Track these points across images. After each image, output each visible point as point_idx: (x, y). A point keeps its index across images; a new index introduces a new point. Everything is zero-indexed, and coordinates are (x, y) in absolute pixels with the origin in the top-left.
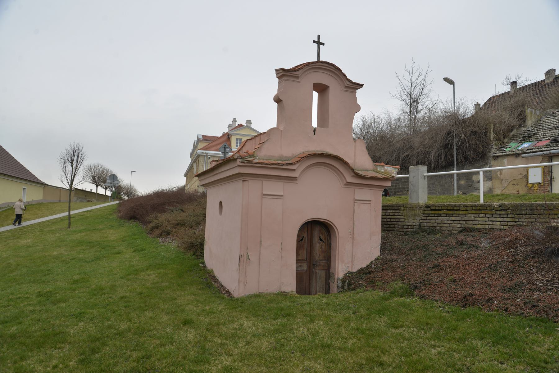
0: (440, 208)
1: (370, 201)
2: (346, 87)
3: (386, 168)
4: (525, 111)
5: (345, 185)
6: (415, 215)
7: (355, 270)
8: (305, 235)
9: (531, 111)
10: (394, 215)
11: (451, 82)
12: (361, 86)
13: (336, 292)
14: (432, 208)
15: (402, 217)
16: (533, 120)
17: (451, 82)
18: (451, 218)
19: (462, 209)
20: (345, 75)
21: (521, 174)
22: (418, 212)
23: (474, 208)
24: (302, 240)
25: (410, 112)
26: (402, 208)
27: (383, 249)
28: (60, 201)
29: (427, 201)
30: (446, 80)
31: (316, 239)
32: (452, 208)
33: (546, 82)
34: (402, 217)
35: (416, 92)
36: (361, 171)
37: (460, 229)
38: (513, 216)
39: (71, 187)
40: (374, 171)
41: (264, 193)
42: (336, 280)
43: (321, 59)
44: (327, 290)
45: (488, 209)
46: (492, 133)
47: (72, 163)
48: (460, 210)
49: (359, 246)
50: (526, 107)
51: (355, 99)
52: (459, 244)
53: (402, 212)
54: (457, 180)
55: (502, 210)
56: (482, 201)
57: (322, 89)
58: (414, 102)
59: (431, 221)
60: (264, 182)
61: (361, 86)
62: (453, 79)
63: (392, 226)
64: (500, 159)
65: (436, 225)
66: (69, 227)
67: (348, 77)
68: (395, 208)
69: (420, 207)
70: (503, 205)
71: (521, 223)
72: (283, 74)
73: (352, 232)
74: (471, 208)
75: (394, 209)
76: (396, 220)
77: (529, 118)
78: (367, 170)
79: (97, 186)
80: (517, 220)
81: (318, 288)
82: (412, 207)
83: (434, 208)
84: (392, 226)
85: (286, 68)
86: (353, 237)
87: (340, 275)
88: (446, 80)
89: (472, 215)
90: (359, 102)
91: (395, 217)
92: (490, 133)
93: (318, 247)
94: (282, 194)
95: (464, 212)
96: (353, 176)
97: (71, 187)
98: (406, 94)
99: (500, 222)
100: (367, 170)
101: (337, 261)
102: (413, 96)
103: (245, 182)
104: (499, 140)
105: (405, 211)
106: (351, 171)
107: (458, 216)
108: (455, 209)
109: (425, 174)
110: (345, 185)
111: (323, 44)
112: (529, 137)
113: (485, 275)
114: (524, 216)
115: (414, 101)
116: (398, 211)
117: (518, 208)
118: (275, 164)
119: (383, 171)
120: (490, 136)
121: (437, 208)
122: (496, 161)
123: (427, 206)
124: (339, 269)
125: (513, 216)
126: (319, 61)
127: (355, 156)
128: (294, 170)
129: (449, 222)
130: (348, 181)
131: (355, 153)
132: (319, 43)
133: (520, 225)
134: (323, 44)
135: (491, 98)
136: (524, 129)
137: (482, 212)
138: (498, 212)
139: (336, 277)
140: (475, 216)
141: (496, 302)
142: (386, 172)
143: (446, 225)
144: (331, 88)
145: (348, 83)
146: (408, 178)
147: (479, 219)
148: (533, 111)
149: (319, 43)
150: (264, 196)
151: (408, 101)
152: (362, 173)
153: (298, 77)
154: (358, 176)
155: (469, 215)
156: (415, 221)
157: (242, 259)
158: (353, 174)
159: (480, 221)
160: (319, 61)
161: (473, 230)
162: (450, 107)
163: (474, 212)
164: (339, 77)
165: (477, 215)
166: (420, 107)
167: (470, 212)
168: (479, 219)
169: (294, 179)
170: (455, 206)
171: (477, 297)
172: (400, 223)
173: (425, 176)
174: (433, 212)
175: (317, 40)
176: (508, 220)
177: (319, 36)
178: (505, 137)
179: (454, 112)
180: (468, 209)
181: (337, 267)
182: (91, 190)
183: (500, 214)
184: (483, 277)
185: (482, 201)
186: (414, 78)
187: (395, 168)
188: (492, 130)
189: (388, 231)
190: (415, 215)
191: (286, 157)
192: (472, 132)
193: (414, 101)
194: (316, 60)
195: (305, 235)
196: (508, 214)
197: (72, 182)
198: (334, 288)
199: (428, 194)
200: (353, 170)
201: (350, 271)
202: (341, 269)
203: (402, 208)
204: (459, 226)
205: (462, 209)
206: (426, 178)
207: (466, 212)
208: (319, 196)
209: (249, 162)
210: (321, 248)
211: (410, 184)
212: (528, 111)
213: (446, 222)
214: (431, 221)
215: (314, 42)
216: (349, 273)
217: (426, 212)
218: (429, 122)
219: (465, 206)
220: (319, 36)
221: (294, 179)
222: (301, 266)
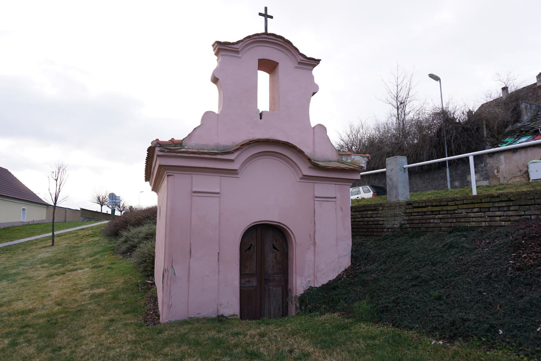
0: (424, 205)
1: (335, 198)
2: (299, 63)
3: (353, 157)
4: (519, 106)
5: (301, 178)
6: (395, 215)
7: (318, 285)
8: (254, 243)
9: (526, 106)
10: (372, 217)
11: (436, 78)
12: (318, 61)
13: (294, 314)
14: (414, 205)
15: (381, 219)
16: (529, 114)
17: (436, 78)
18: (437, 217)
19: (449, 203)
20: (296, 49)
21: (520, 171)
22: (398, 211)
23: (465, 202)
24: (249, 248)
25: (398, 114)
26: (381, 208)
27: (354, 258)
28: (65, 221)
29: (409, 198)
30: (432, 76)
31: (268, 247)
32: (438, 204)
33: (538, 85)
34: (381, 219)
35: (403, 95)
36: (323, 162)
37: (450, 229)
38: (517, 208)
39: (55, 204)
40: (338, 162)
41: (194, 190)
42: (293, 299)
43: (269, 31)
44: (285, 313)
45: (483, 201)
46: (485, 129)
47: (56, 180)
48: (447, 205)
49: (323, 252)
50: (520, 101)
51: (312, 77)
52: (447, 247)
53: (380, 212)
54: (451, 182)
55: (501, 201)
56: (475, 193)
57: (269, 66)
58: (401, 105)
59: (415, 222)
60: (194, 176)
61: (318, 61)
62: (438, 76)
63: (369, 230)
64: (496, 156)
65: (420, 225)
66: (53, 245)
67: (301, 52)
68: (373, 208)
69: (400, 205)
70: (502, 194)
71: (529, 217)
72: (222, 48)
73: (312, 237)
74: (461, 202)
75: (371, 210)
76: (375, 223)
77: (524, 112)
78: (330, 161)
79: (102, 206)
80: (523, 213)
81: (272, 309)
82: (391, 206)
83: (417, 205)
84: (369, 230)
85: (222, 41)
86: (315, 244)
87: (298, 292)
88: (432, 76)
89: (464, 211)
90: (316, 81)
91: (373, 219)
92: (483, 129)
93: (271, 257)
94: (218, 191)
95: (453, 208)
96: (310, 168)
97: (55, 204)
98: (392, 96)
99: (500, 216)
100: (330, 161)
101: (294, 275)
102: (400, 99)
103: (169, 177)
104: (493, 136)
105: (384, 211)
106: (307, 161)
107: (445, 212)
108: (443, 204)
109: (405, 166)
110: (301, 178)
111: (271, 17)
112: (527, 131)
113: (482, 290)
114: (532, 208)
115: (401, 103)
116: (376, 212)
117: (523, 196)
118: (206, 153)
119: (349, 161)
120: (483, 132)
121: (420, 205)
122: (492, 158)
123: (409, 204)
124: (297, 284)
125: (517, 208)
126: (266, 33)
127: (314, 144)
128: (232, 161)
129: (436, 221)
130: (305, 174)
131: (314, 140)
132: (266, 16)
133: (528, 219)
134: (271, 17)
135: (483, 105)
136: (519, 125)
137: (476, 205)
138: (497, 205)
139: (294, 294)
140: (467, 211)
141: (501, 332)
142: (353, 163)
143: (432, 225)
144: (280, 65)
145: (302, 58)
146: (384, 173)
147: (472, 215)
148: (529, 106)
149: (266, 16)
150: (193, 194)
151: (395, 103)
152: (321, 164)
153: (237, 52)
154: (315, 166)
155: (460, 211)
156: (396, 222)
157: (166, 275)
158: (310, 165)
159: (475, 218)
160: (266, 33)
161: (467, 229)
162: (438, 105)
163: (465, 206)
164: (290, 52)
165: (470, 210)
166: (407, 110)
167: (460, 207)
168: (472, 215)
169: (233, 172)
170: (441, 201)
171: (471, 324)
172: (379, 226)
173: (405, 169)
174: (416, 210)
175: (263, 12)
176: (510, 213)
177: (266, 9)
178: (499, 133)
179: (443, 108)
180: (458, 203)
181: (294, 281)
182: (107, 212)
183: (499, 207)
184: (480, 293)
185: (475, 193)
186: (400, 81)
187: (364, 157)
188: (484, 126)
189: (366, 236)
190: (395, 215)
191: (224, 146)
192: (463, 128)
193: (401, 103)
194: (264, 31)
195: (254, 243)
196: (509, 206)
197: (56, 200)
198: (293, 309)
199: (410, 192)
200: (309, 160)
201: (312, 286)
202: (300, 284)
203: (381, 208)
204: (448, 225)
205: (449, 203)
206: (407, 171)
207: (456, 207)
208: (266, 194)
209: (171, 151)
210: (275, 258)
211: (388, 179)
212: (523, 106)
213: (432, 221)
214: (415, 222)
215: (260, 14)
216: (311, 288)
217: (408, 211)
218: (419, 125)
219: (454, 200)
220: (266, 9)
221: (233, 172)
222: (249, 281)
